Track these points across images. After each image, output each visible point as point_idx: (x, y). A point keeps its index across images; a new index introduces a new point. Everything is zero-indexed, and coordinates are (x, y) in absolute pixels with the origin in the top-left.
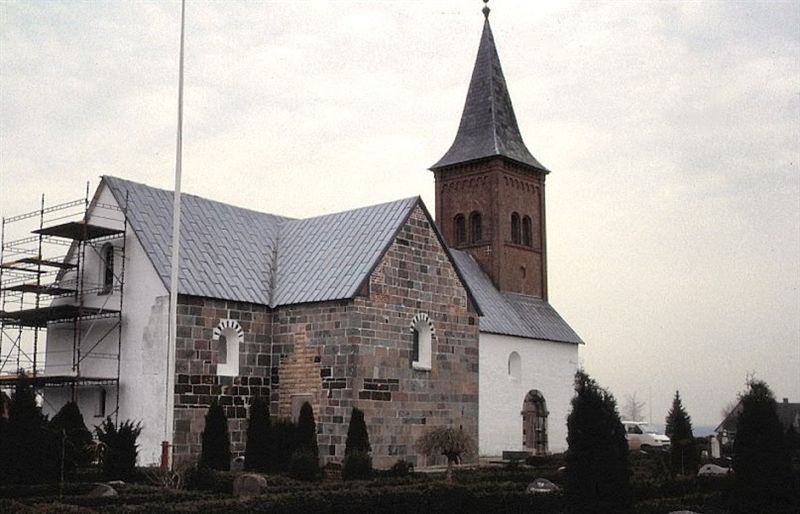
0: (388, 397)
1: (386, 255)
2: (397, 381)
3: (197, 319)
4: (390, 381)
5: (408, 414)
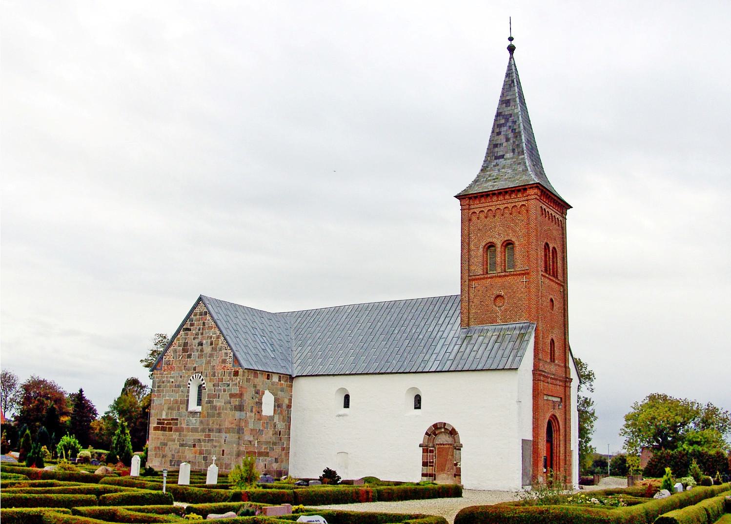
0: (170, 429)
1: (175, 341)
2: (177, 419)
3: (177, 425)
4: (172, 419)
5: (183, 441)
